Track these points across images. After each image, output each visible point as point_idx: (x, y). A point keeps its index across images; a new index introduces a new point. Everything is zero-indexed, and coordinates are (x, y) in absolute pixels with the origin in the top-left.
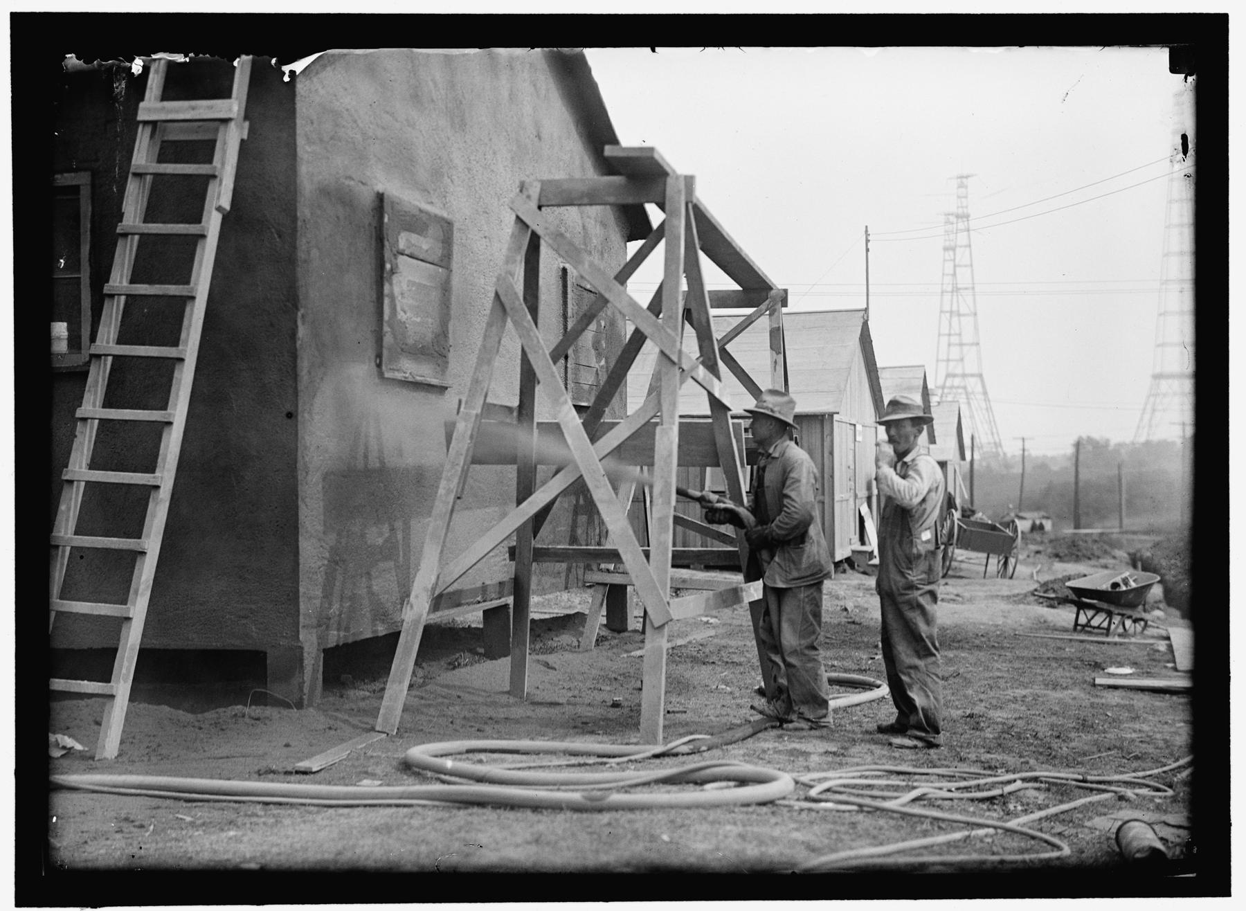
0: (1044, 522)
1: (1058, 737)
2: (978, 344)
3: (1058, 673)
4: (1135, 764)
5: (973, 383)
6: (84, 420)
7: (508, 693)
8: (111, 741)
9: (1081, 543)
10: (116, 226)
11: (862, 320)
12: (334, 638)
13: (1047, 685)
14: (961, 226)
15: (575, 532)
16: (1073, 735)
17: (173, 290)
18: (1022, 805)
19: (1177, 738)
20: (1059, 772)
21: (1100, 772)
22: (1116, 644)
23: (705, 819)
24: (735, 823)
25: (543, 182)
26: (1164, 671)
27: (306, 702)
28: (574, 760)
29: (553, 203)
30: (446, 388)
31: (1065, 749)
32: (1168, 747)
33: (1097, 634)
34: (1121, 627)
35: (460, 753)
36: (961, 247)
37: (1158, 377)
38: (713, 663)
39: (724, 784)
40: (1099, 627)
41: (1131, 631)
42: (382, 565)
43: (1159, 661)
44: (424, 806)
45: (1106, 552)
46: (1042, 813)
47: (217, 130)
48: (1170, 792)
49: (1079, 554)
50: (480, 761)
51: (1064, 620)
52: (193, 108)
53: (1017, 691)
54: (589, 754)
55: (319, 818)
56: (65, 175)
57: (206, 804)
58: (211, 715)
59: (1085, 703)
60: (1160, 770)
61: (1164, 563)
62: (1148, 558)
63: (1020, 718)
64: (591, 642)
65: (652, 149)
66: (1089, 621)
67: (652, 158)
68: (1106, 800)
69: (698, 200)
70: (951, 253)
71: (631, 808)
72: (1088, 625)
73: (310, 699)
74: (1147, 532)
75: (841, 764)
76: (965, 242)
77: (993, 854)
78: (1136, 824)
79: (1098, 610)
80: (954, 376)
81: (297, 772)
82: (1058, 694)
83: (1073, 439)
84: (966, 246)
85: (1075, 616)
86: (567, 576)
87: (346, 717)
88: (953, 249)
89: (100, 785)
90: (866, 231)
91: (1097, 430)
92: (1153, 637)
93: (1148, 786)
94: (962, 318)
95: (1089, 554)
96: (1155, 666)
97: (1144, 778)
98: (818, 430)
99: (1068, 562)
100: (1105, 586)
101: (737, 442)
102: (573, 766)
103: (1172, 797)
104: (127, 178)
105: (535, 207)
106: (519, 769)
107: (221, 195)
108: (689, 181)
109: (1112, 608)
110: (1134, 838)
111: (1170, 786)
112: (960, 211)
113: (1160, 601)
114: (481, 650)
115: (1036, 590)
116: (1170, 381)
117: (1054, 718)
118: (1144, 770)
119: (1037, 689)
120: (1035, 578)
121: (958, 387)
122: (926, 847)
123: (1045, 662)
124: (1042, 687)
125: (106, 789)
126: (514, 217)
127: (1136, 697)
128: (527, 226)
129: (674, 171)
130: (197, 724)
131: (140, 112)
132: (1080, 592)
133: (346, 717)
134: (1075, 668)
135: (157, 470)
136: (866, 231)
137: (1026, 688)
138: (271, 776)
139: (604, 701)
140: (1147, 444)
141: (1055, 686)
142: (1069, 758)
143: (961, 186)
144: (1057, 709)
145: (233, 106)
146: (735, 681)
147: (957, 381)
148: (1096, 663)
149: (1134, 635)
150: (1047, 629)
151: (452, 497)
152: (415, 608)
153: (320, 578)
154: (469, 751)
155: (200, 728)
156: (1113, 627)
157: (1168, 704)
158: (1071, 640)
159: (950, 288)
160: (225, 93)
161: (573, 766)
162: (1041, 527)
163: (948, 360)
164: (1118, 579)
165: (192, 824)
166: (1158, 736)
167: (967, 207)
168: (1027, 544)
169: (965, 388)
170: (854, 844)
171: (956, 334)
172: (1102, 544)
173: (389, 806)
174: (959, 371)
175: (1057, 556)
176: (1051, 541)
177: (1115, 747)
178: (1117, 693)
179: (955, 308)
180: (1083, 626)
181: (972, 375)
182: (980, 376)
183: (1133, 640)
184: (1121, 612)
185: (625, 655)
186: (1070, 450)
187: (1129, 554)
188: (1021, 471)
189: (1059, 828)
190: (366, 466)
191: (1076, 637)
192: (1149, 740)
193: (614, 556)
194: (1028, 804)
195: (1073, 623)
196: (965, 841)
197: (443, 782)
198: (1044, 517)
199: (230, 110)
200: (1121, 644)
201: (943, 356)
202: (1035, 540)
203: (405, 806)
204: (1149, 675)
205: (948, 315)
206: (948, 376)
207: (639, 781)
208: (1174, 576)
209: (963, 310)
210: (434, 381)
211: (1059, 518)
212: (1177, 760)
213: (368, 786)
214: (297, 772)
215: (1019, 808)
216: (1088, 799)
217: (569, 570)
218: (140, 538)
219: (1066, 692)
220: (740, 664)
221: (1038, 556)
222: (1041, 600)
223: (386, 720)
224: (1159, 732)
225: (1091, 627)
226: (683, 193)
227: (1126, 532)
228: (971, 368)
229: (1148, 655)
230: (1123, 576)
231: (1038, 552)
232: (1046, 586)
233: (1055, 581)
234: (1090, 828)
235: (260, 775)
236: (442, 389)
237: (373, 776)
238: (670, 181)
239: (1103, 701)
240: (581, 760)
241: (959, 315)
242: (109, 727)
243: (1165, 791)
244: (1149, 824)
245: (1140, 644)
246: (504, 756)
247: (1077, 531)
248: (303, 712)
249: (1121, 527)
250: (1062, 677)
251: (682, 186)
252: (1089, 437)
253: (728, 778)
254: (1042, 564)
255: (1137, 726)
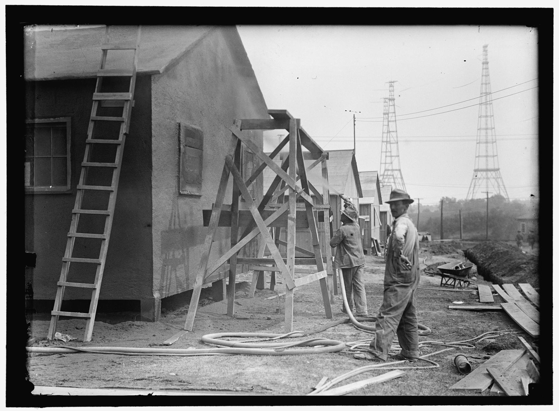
0: (428, 236)
1: (435, 328)
2: (398, 156)
3: (435, 304)
4: (462, 338)
5: (396, 173)
6: (75, 214)
7: (226, 315)
8: (89, 336)
9: (444, 247)
10: (86, 140)
11: (352, 154)
12: (165, 294)
13: (430, 309)
14: (391, 103)
15: (245, 250)
16: (440, 327)
17: (109, 165)
18: (423, 352)
19: (478, 328)
20: (435, 341)
21: (450, 341)
22: (457, 291)
23: (319, 357)
24: (329, 358)
25: (242, 120)
26: (475, 303)
27: (156, 319)
28: (262, 339)
29: (246, 128)
30: (201, 196)
31: (437, 333)
32: (474, 331)
33: (450, 288)
34: (459, 284)
35: (219, 338)
36: (391, 113)
37: (476, 171)
38: (301, 302)
39: (321, 346)
40: (450, 285)
41: (463, 286)
42: (180, 266)
43: (473, 299)
44: (218, 355)
45: (454, 250)
46: (430, 354)
47: (124, 104)
48: (474, 347)
49: (443, 251)
50: (228, 340)
51: (437, 282)
52: (115, 96)
53: (420, 311)
54: (266, 337)
55: (182, 359)
56: (61, 118)
57: (138, 356)
58: (119, 325)
59: (445, 316)
60: (471, 340)
61: (478, 255)
62: (472, 253)
63: (421, 322)
64: (253, 294)
65: (285, 111)
66: (447, 282)
67: (286, 114)
68: (452, 350)
69: (302, 128)
70: (387, 116)
71: (292, 354)
72: (446, 284)
73: (157, 318)
74: (472, 240)
75: (357, 339)
76: (393, 111)
77: (414, 366)
78: (461, 356)
79: (450, 278)
80: (388, 170)
81: (164, 345)
82: (435, 312)
83: (439, 200)
84: (393, 113)
85: (441, 280)
86: (242, 267)
87: (171, 325)
88: (388, 114)
89: (95, 350)
90: (354, 117)
91: (450, 195)
92: (472, 288)
93: (466, 345)
94: (391, 145)
95: (447, 251)
96: (472, 301)
97: (465, 342)
98: (335, 203)
99: (438, 255)
100: (453, 268)
101: (315, 218)
102: (261, 341)
103: (475, 348)
104: (89, 122)
105: (240, 130)
106: (245, 342)
107: (124, 129)
108: (298, 121)
109: (456, 277)
110: (460, 360)
111: (474, 345)
112: (391, 97)
113: (476, 273)
114: (211, 298)
115: (425, 269)
116: (482, 173)
117: (433, 321)
118: (465, 340)
119: (427, 310)
120: (425, 263)
121: (390, 175)
122: (392, 365)
123: (429, 299)
124: (429, 310)
125: (98, 352)
126: (232, 133)
127: (464, 313)
128: (237, 137)
129: (292, 117)
130: (115, 328)
131: (94, 97)
132: (443, 270)
133: (171, 325)
134: (441, 302)
135: (104, 233)
136: (354, 117)
137: (423, 310)
138: (155, 346)
139: (264, 317)
140: (472, 200)
141: (434, 309)
142: (439, 336)
143: (391, 86)
144: (435, 318)
145: (129, 95)
146: (311, 309)
147: (389, 173)
148: (449, 300)
149: (464, 288)
150: (430, 286)
151: (211, 240)
152: (198, 283)
153: (160, 272)
154: (222, 337)
155: (117, 330)
156: (456, 284)
157: (476, 315)
158: (439, 290)
159: (386, 131)
160: (127, 91)
161: (261, 341)
162: (427, 239)
163: (386, 163)
164: (458, 265)
165: (137, 362)
166: (471, 327)
167: (394, 96)
168: (421, 247)
169: (393, 175)
170: (369, 364)
171: (389, 152)
172: (452, 247)
173: (206, 355)
174: (390, 168)
175: (434, 252)
176: (431, 246)
177: (455, 332)
178: (457, 311)
179: (388, 140)
180: (444, 284)
181: (396, 170)
182: (400, 170)
183: (464, 290)
184: (459, 278)
185: (266, 299)
186: (439, 204)
187: (463, 251)
188: (418, 213)
189: (435, 359)
190: (175, 228)
191: (442, 289)
192: (468, 329)
193: (272, 262)
194: (425, 352)
195: (440, 283)
196: (405, 363)
197: (219, 347)
198: (428, 234)
199: (129, 97)
200: (459, 292)
201: (383, 161)
202: (424, 245)
203: (211, 355)
204: (469, 304)
205: (385, 143)
206: (386, 170)
207: (290, 345)
208: (482, 261)
209: (392, 140)
210: (197, 194)
211: (433, 234)
212: (477, 336)
213: (191, 349)
214: (164, 345)
215: (422, 353)
216: (446, 350)
217: (243, 265)
218: (98, 258)
219: (437, 311)
220: (311, 302)
221: (426, 252)
222: (427, 273)
223: (188, 325)
224: (471, 326)
225: (447, 284)
226: (296, 126)
227: (463, 240)
228: (395, 166)
229: (469, 296)
230: (460, 264)
231: (426, 251)
232: (430, 268)
233: (433, 265)
234: (446, 359)
235: (151, 346)
236: (199, 196)
237: (192, 346)
238: (291, 121)
239: (451, 315)
240: (264, 339)
241: (390, 143)
242: (88, 329)
243: (473, 347)
244: (466, 358)
245: (466, 292)
246: (235, 338)
247: (442, 240)
248: (155, 323)
249: (461, 238)
250: (436, 305)
251: (295, 123)
252: (447, 197)
253: (321, 344)
254: (427, 256)
255: (464, 324)
